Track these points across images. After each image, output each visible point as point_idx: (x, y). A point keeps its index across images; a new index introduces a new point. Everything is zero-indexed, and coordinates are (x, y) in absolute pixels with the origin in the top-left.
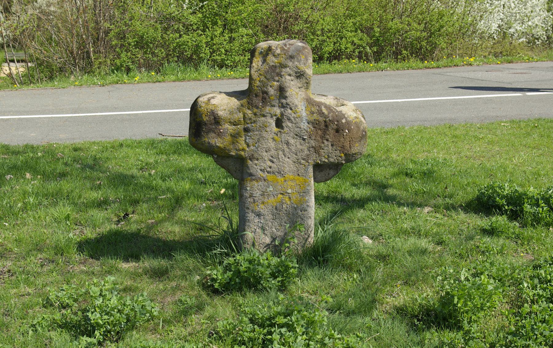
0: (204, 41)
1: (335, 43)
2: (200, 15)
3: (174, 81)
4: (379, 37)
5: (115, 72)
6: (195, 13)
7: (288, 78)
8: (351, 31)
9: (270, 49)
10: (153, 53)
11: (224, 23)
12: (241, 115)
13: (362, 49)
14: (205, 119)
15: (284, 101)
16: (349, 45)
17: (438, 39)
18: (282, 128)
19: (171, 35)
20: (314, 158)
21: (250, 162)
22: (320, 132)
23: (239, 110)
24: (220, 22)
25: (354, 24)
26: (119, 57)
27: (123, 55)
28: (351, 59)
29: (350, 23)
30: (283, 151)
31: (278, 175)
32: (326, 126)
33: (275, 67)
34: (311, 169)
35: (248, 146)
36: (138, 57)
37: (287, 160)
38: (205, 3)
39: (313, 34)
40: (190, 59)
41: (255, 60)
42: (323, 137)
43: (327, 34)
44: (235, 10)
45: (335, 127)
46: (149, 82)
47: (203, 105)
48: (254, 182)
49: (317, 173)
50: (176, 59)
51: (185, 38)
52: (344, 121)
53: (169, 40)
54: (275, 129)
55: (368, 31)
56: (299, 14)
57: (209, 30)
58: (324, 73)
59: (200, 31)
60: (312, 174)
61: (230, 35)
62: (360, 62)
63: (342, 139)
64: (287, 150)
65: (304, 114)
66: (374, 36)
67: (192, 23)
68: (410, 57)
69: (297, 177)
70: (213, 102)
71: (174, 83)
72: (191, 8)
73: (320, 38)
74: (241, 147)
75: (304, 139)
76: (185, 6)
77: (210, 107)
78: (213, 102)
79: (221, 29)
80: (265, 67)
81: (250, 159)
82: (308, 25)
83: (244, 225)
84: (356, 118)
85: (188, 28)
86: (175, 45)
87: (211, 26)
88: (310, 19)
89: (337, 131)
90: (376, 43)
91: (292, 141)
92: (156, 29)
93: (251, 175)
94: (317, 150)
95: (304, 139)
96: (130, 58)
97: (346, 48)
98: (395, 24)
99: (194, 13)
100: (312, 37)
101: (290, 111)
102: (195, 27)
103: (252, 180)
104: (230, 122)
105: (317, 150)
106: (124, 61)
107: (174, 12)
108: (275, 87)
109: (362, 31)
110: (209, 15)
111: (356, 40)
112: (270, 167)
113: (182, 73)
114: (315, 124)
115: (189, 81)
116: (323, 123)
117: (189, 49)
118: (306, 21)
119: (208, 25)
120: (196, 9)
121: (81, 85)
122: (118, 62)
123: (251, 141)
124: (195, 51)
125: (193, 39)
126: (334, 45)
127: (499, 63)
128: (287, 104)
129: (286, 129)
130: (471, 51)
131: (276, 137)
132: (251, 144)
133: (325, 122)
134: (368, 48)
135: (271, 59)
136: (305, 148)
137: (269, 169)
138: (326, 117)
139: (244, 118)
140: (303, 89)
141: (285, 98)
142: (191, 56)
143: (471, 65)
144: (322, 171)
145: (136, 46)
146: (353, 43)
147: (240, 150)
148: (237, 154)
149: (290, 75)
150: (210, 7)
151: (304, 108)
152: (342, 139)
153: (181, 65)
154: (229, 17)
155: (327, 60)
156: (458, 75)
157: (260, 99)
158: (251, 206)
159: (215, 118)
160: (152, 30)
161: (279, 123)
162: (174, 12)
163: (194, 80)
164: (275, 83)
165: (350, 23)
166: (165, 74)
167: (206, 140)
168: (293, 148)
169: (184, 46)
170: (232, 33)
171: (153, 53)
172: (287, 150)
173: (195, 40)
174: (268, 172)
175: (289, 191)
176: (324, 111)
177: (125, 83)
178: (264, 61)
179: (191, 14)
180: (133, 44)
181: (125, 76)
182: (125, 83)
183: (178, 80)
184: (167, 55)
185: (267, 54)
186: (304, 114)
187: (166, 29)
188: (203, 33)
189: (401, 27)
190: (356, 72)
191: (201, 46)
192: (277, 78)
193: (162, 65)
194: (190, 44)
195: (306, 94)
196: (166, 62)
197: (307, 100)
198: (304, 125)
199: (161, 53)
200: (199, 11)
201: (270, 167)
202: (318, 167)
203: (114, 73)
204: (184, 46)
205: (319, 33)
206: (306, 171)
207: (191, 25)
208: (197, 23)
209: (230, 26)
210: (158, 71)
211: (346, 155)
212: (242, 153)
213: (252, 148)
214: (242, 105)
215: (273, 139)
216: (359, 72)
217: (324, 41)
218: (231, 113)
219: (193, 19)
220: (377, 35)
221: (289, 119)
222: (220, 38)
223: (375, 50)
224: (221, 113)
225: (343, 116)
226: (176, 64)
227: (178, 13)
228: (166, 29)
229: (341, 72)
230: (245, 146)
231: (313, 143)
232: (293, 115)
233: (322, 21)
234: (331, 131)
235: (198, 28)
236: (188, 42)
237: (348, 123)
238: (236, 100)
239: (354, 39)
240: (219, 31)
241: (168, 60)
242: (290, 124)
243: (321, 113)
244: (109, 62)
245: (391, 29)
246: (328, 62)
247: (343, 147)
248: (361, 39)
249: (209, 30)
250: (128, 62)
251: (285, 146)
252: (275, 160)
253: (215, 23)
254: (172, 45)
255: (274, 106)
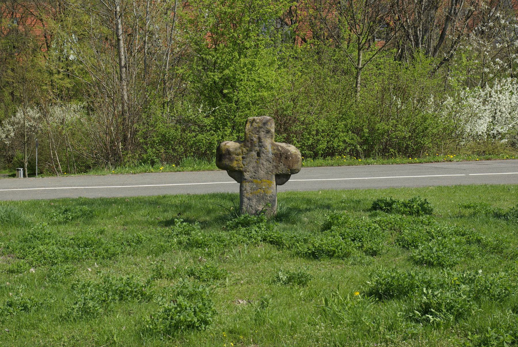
0: (216, 139)
1: (328, 142)
2: (213, 118)
3: (192, 171)
4: (368, 137)
5: (143, 164)
6: (209, 116)
7: (263, 133)
8: (343, 132)
9: (254, 120)
10: (174, 150)
11: (232, 124)
12: (241, 151)
13: (353, 148)
14: (224, 152)
15: (261, 144)
16: (341, 144)
17: (422, 139)
18: (260, 156)
19: (189, 134)
20: (275, 171)
21: (245, 173)
22: (278, 158)
23: (240, 148)
24: (229, 124)
25: (346, 126)
26: (146, 152)
27: (149, 150)
28: (343, 155)
29: (341, 125)
30: (261, 168)
31: (258, 179)
32: (281, 156)
33: (256, 128)
34: (274, 177)
35: (244, 165)
36: (161, 152)
37: (262, 172)
38: (217, 108)
39: (309, 134)
40: (205, 154)
41: (247, 125)
42: (279, 161)
43: (322, 134)
44: (242, 113)
45: (285, 156)
46: (171, 171)
47: (223, 146)
48: (247, 183)
49: (277, 179)
50: (192, 154)
51: (200, 136)
52: (289, 153)
53: (187, 138)
54: (257, 157)
55: (358, 131)
56: (297, 117)
57: (220, 130)
58: (318, 166)
59: (212, 131)
60: (274, 179)
61: (238, 135)
62: (351, 158)
63: (288, 162)
64: (262, 167)
65: (270, 150)
66: (364, 136)
67: (206, 124)
68: (397, 154)
69: (267, 181)
70: (227, 145)
71: (191, 172)
72: (205, 113)
73: (315, 137)
74: (241, 166)
75: (270, 162)
76: (200, 110)
77: (226, 147)
78: (227, 145)
79: (230, 130)
80: (252, 128)
81: (245, 172)
82: (305, 126)
83: (242, 204)
84: (295, 152)
85: (202, 129)
86: (192, 142)
87: (222, 127)
88: (307, 121)
89: (286, 158)
90: (365, 142)
91: (265, 163)
92: (177, 130)
93: (245, 179)
94: (277, 167)
95: (270, 162)
96: (155, 153)
97: (339, 146)
98: (381, 126)
99: (207, 116)
100: (308, 136)
101: (263, 149)
102: (208, 128)
103: (246, 182)
104: (236, 154)
105: (277, 167)
106: (150, 156)
107: (191, 115)
108: (257, 138)
109: (353, 132)
110: (220, 118)
111: (347, 140)
112: (255, 176)
113: (198, 165)
114: (275, 155)
115: (203, 171)
116: (279, 154)
117: (204, 146)
118: (303, 123)
119: (219, 126)
120: (209, 113)
121: (117, 173)
122: (145, 156)
123: (245, 163)
124: (208, 147)
125: (207, 137)
126: (327, 143)
127: (478, 160)
128: (262, 145)
129: (262, 157)
130: (457, 150)
131: (257, 161)
132: (245, 164)
133: (280, 154)
134: (359, 146)
135: (255, 124)
136: (271, 166)
137: (254, 177)
138: (281, 151)
139: (242, 152)
140: (270, 139)
141: (261, 142)
142: (206, 151)
143: (450, 161)
144: (279, 178)
145: (160, 143)
146: (344, 142)
147: (240, 167)
148: (239, 169)
149: (263, 132)
150: (221, 111)
151: (270, 147)
152: (288, 162)
153: (197, 159)
154: (238, 119)
155: (321, 156)
156: (429, 166)
157: (250, 143)
158: (246, 195)
159: (228, 152)
160: (172, 131)
161: (259, 154)
162: (191, 115)
163: (208, 170)
164: (257, 136)
165: (341, 125)
166: (183, 166)
167: (224, 162)
168: (265, 167)
169: (200, 143)
170: (239, 133)
171: (174, 150)
172: (262, 167)
173: (208, 138)
174: (254, 178)
175: (264, 187)
176: (280, 148)
177: (152, 172)
178: (251, 125)
179: (205, 117)
180: (157, 141)
181: (150, 167)
182: (152, 172)
183: (195, 170)
184: (186, 151)
185: (253, 122)
186: (270, 150)
187: (184, 130)
188: (215, 133)
189: (386, 128)
190: (346, 166)
191: (214, 143)
192: (257, 133)
193: (180, 158)
194: (204, 141)
195: (272, 141)
196: (184, 156)
197: (272, 144)
198: (270, 155)
199: (181, 149)
200: (212, 115)
201: (255, 176)
202: (277, 176)
203: (141, 165)
204: (200, 143)
205: (314, 133)
206: (272, 177)
207: (206, 126)
208: (210, 125)
209: (238, 127)
210: (177, 164)
211: (290, 170)
212: (241, 169)
213: (246, 166)
214: (241, 146)
215: (256, 162)
216: (349, 165)
217: (319, 140)
218: (236, 149)
219: (207, 121)
220: (366, 135)
221: (263, 153)
222: (230, 137)
223: (365, 148)
224: (231, 150)
225: (289, 151)
226: (193, 158)
227: (194, 116)
228: (184, 130)
229: (332, 166)
230: (243, 166)
231: (275, 164)
232: (265, 150)
233: (316, 123)
234: (283, 158)
235: (211, 129)
236: (202, 140)
237: (291, 154)
238: (238, 144)
239: (346, 138)
240: (229, 131)
241: (185, 155)
242: (264, 155)
243: (278, 150)
244: (137, 156)
245: (378, 129)
246: (322, 158)
247: (289, 166)
248: (352, 139)
249: (220, 130)
250: (153, 156)
251: (262, 165)
252: (257, 172)
253: (226, 125)
254: (189, 143)
255: (256, 146)
